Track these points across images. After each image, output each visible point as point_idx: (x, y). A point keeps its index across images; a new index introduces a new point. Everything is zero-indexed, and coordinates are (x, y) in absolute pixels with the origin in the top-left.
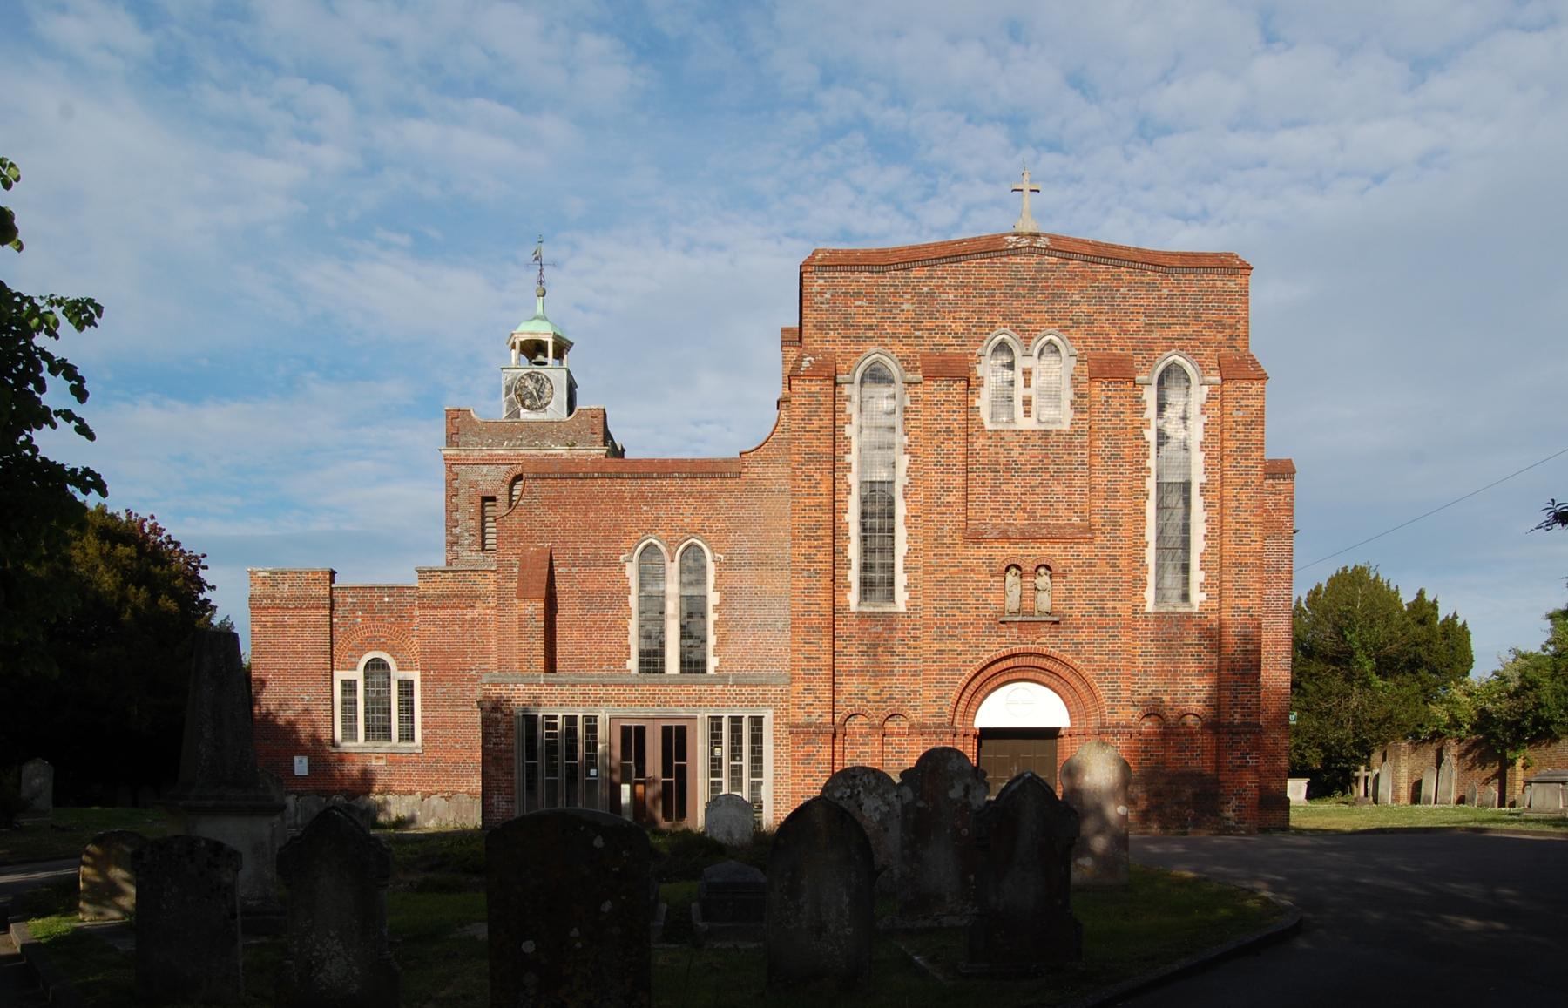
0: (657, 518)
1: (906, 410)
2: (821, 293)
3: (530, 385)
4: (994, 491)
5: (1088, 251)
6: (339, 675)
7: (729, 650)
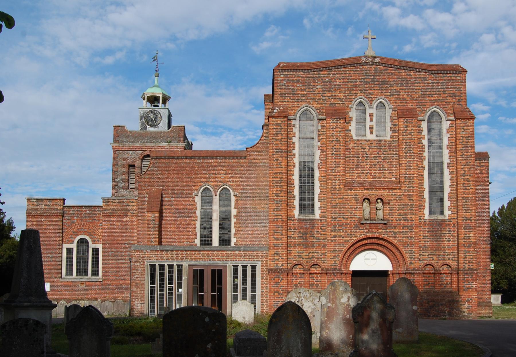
0: (209, 176)
1: (319, 131)
2: (282, 81)
3: (151, 115)
4: (358, 166)
5: (396, 64)
6: (65, 246)
7: (241, 235)
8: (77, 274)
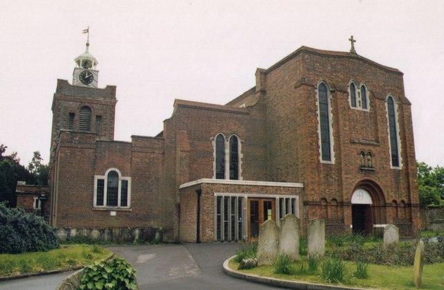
6: (97, 177)
8: (108, 204)
